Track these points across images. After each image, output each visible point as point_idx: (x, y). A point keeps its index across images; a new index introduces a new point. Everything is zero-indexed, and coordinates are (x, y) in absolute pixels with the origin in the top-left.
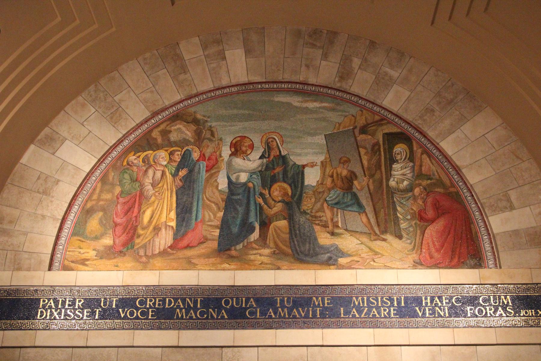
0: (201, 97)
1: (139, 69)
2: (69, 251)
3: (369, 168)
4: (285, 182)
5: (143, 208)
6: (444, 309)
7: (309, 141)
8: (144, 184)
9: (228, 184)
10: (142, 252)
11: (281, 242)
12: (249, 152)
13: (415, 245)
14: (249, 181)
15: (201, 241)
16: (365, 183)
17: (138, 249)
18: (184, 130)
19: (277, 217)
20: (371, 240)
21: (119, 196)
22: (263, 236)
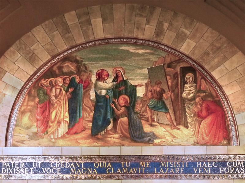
0: (79, 47)
1: (43, 31)
2: (15, 136)
3: (172, 87)
4: (126, 95)
5: (51, 110)
6: (208, 169)
7: (139, 72)
8: (51, 96)
9: (96, 95)
10: (52, 137)
11: (124, 130)
12: (106, 78)
13: (195, 132)
14: (107, 94)
15: (82, 130)
16: (169, 95)
17: (50, 134)
18: (71, 66)
19: (122, 115)
20: (172, 129)
21: (38, 103)
22: (115, 126)
